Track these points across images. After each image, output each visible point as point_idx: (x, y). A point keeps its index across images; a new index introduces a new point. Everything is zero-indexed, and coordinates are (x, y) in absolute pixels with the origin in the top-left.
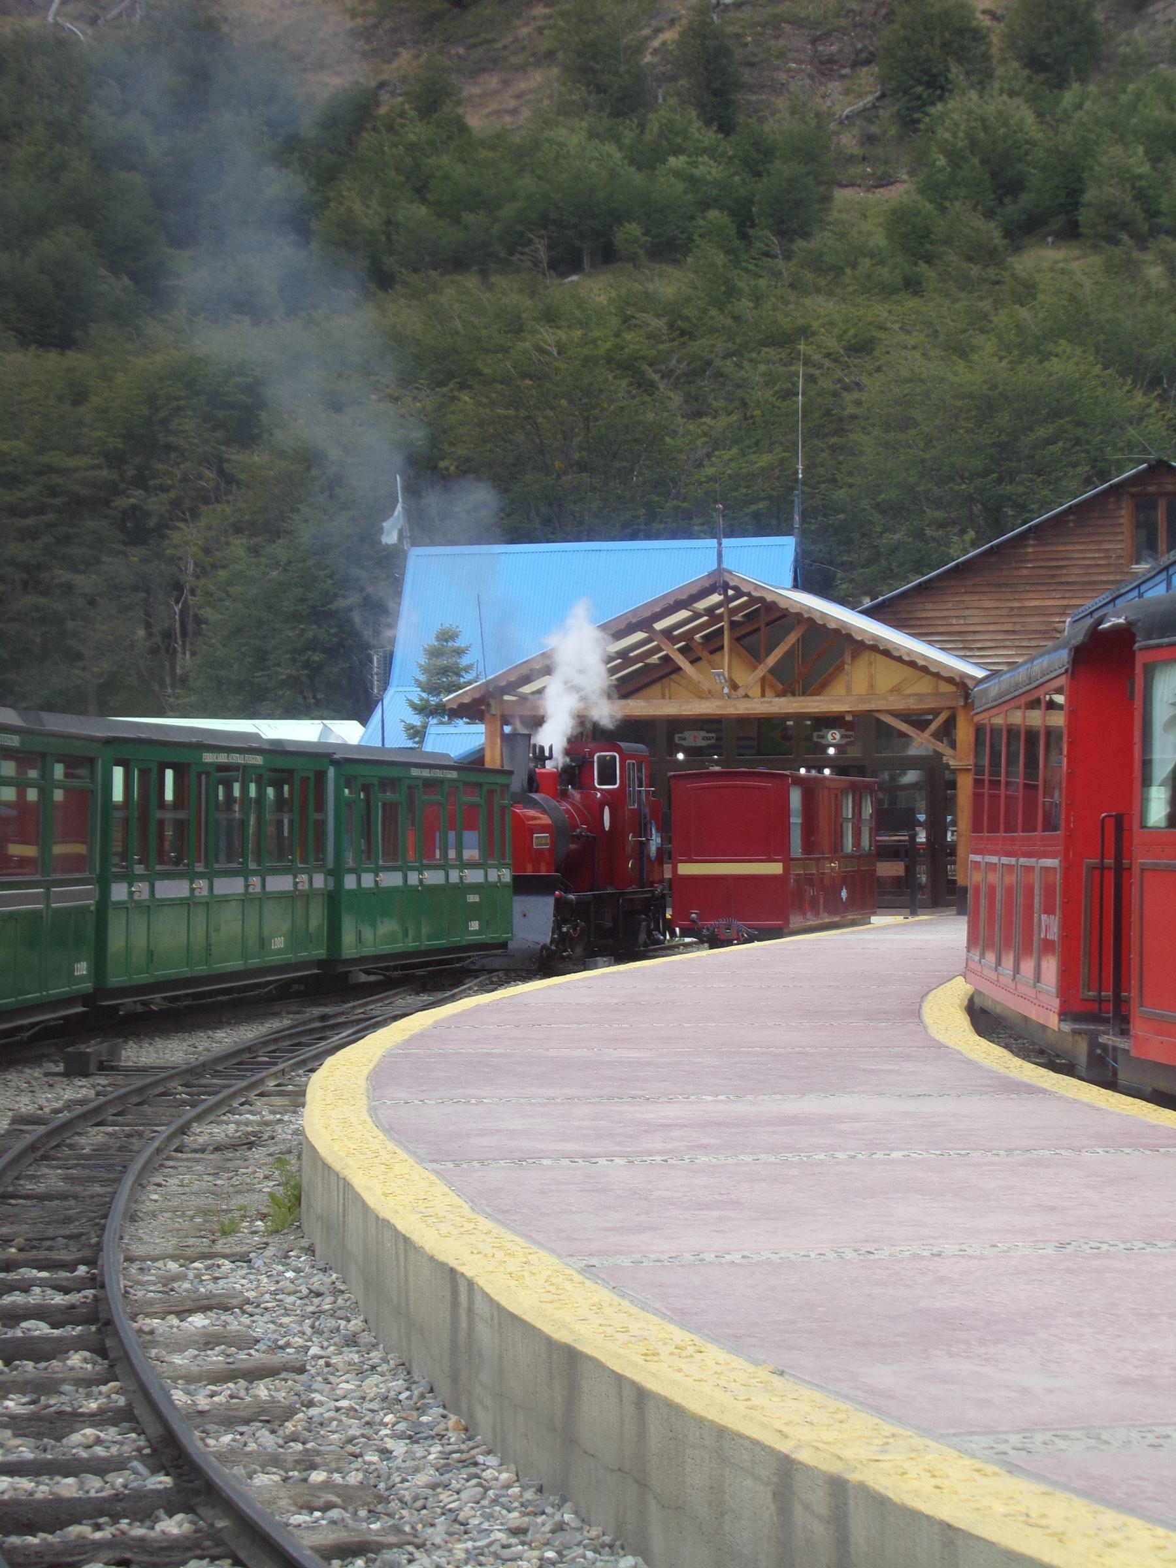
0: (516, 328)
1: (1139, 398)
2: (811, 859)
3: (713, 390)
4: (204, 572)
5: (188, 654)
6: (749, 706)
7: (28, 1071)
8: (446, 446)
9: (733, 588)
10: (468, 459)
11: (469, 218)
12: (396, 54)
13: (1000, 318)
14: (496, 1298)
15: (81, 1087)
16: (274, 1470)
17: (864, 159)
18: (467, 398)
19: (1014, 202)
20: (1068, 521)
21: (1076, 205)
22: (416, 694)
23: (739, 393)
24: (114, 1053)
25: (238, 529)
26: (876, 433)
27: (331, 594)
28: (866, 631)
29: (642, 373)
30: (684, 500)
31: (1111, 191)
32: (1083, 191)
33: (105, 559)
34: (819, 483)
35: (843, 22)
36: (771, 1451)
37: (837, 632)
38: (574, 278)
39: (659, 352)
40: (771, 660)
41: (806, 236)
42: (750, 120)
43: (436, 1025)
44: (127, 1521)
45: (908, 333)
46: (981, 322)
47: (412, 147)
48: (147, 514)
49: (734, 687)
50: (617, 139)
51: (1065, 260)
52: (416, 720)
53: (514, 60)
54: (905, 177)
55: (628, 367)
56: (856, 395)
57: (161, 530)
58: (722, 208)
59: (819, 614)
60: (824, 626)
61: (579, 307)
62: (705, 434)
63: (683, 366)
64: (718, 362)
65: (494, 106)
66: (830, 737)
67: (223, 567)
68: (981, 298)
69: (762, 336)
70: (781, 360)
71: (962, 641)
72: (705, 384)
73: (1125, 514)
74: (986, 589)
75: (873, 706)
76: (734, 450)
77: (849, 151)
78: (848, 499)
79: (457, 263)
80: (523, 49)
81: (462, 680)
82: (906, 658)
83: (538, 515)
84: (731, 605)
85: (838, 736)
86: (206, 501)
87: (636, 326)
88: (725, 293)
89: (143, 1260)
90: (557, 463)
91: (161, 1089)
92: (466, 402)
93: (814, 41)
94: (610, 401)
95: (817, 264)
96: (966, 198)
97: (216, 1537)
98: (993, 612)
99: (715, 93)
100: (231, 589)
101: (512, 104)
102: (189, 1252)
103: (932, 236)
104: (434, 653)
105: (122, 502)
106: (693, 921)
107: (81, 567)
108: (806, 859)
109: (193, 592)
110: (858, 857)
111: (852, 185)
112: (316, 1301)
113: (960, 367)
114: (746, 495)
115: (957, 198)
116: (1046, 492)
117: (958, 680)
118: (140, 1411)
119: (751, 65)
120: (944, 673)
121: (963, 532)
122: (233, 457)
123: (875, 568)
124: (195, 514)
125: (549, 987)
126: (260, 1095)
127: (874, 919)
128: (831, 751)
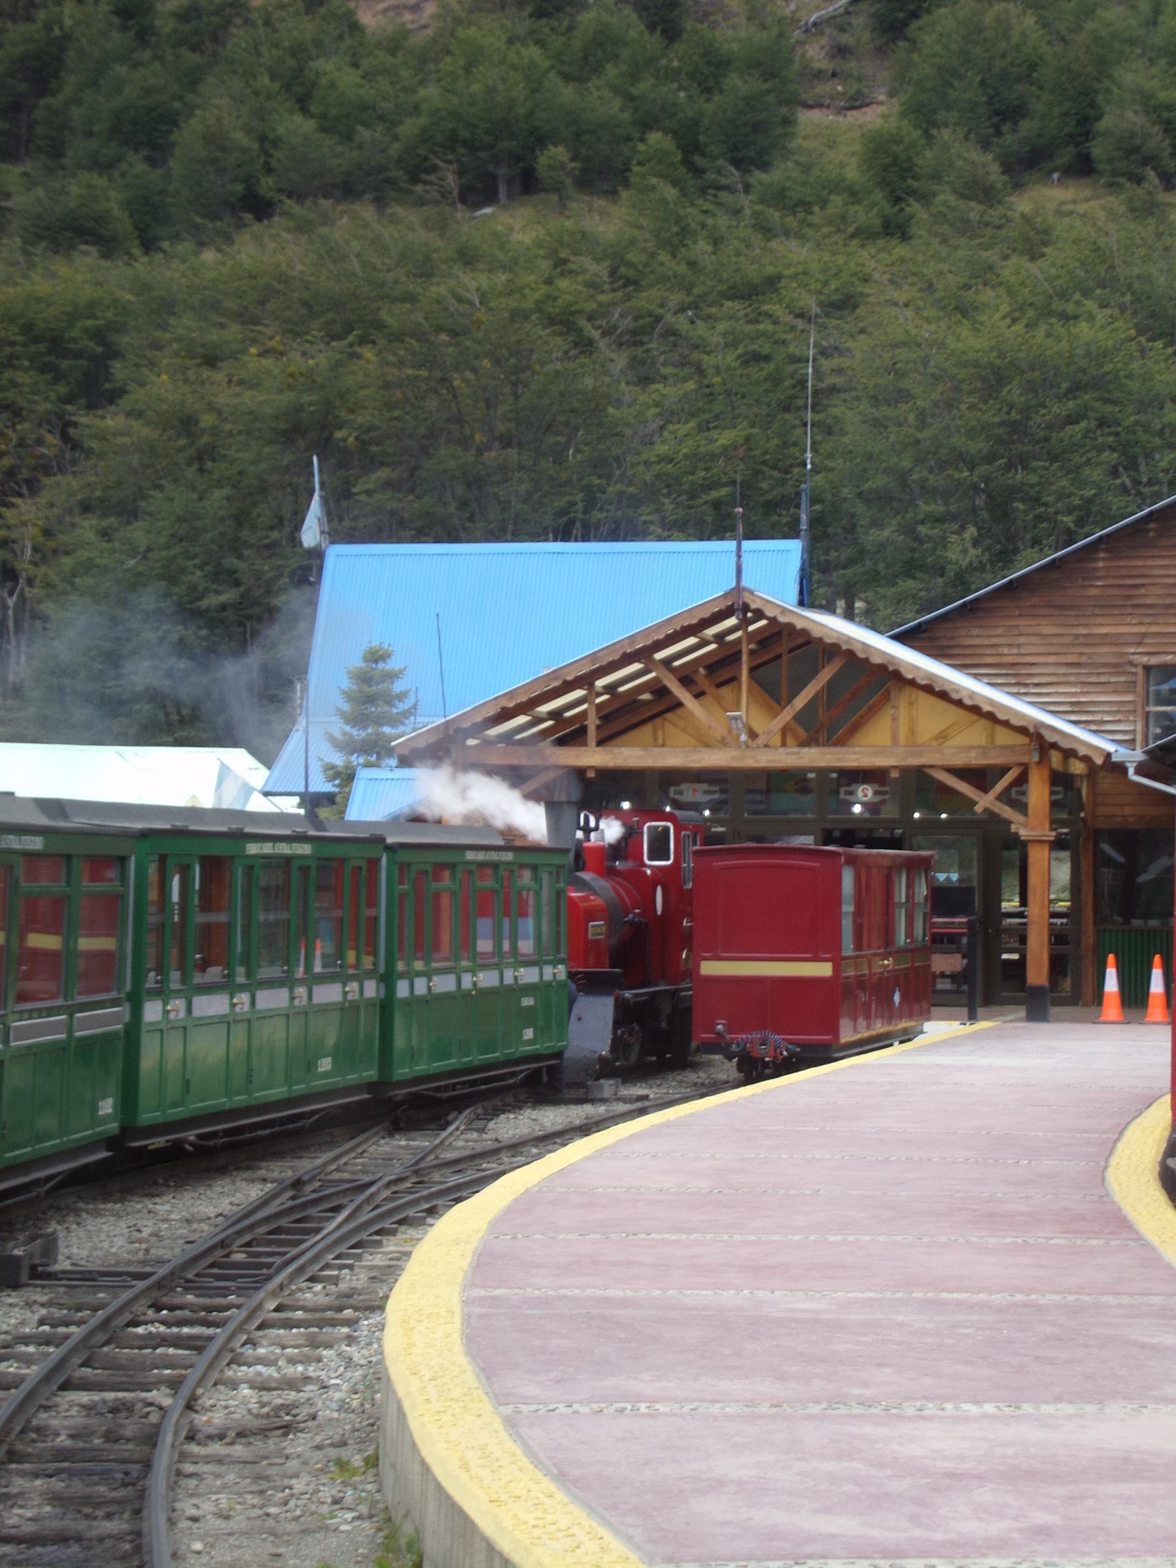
0: (425, 271)
2: (862, 956)
3: (663, 353)
4: (44, 560)
5: (23, 657)
6: (770, 758)
8: (343, 414)
9: (753, 611)
10: (370, 429)
11: (364, 134)
15: (11, 1305)
17: (834, 75)
18: (369, 355)
19: (1014, 131)
20: (1148, 531)
21: (1088, 135)
22: (338, 728)
23: (695, 356)
24: (50, 1247)
25: (86, 508)
26: (862, 408)
27: (200, 588)
28: (918, 669)
29: (579, 330)
30: (630, 484)
32: (1099, 118)
34: (792, 466)
37: (882, 668)
38: (488, 210)
39: (600, 304)
40: (800, 702)
41: (764, 166)
42: (699, 26)
43: (497, 1225)
46: (984, 274)
47: (297, 50)
49: (753, 735)
50: (541, 43)
51: (1074, 202)
52: (338, 760)
54: (882, 98)
56: (836, 361)
58: (666, 131)
59: (860, 646)
60: (866, 660)
61: (501, 247)
62: (657, 405)
63: (628, 322)
64: (669, 318)
66: (860, 793)
67: (67, 553)
69: (725, 287)
70: (746, 315)
71: (1016, 675)
74: (1043, 611)
76: (692, 424)
77: (816, 65)
78: (827, 487)
79: (347, 190)
81: (395, 711)
82: (968, 702)
83: (454, 498)
84: (751, 628)
85: (870, 793)
86: (47, 471)
87: (570, 271)
88: (677, 234)
90: (477, 436)
91: (127, 1317)
92: (368, 361)
94: (543, 363)
95: (778, 197)
96: (956, 124)
98: (1054, 640)
100: (78, 580)
103: (917, 169)
106: (719, 1034)
108: (857, 957)
110: (912, 951)
111: (820, 106)
114: (705, 479)
115: (946, 125)
116: (1064, 482)
117: (1032, 730)
120: (1015, 722)
121: (963, 528)
122: (83, 420)
123: (857, 569)
124: (33, 487)
125: (599, 1154)
126: (260, 1328)
127: (928, 1026)
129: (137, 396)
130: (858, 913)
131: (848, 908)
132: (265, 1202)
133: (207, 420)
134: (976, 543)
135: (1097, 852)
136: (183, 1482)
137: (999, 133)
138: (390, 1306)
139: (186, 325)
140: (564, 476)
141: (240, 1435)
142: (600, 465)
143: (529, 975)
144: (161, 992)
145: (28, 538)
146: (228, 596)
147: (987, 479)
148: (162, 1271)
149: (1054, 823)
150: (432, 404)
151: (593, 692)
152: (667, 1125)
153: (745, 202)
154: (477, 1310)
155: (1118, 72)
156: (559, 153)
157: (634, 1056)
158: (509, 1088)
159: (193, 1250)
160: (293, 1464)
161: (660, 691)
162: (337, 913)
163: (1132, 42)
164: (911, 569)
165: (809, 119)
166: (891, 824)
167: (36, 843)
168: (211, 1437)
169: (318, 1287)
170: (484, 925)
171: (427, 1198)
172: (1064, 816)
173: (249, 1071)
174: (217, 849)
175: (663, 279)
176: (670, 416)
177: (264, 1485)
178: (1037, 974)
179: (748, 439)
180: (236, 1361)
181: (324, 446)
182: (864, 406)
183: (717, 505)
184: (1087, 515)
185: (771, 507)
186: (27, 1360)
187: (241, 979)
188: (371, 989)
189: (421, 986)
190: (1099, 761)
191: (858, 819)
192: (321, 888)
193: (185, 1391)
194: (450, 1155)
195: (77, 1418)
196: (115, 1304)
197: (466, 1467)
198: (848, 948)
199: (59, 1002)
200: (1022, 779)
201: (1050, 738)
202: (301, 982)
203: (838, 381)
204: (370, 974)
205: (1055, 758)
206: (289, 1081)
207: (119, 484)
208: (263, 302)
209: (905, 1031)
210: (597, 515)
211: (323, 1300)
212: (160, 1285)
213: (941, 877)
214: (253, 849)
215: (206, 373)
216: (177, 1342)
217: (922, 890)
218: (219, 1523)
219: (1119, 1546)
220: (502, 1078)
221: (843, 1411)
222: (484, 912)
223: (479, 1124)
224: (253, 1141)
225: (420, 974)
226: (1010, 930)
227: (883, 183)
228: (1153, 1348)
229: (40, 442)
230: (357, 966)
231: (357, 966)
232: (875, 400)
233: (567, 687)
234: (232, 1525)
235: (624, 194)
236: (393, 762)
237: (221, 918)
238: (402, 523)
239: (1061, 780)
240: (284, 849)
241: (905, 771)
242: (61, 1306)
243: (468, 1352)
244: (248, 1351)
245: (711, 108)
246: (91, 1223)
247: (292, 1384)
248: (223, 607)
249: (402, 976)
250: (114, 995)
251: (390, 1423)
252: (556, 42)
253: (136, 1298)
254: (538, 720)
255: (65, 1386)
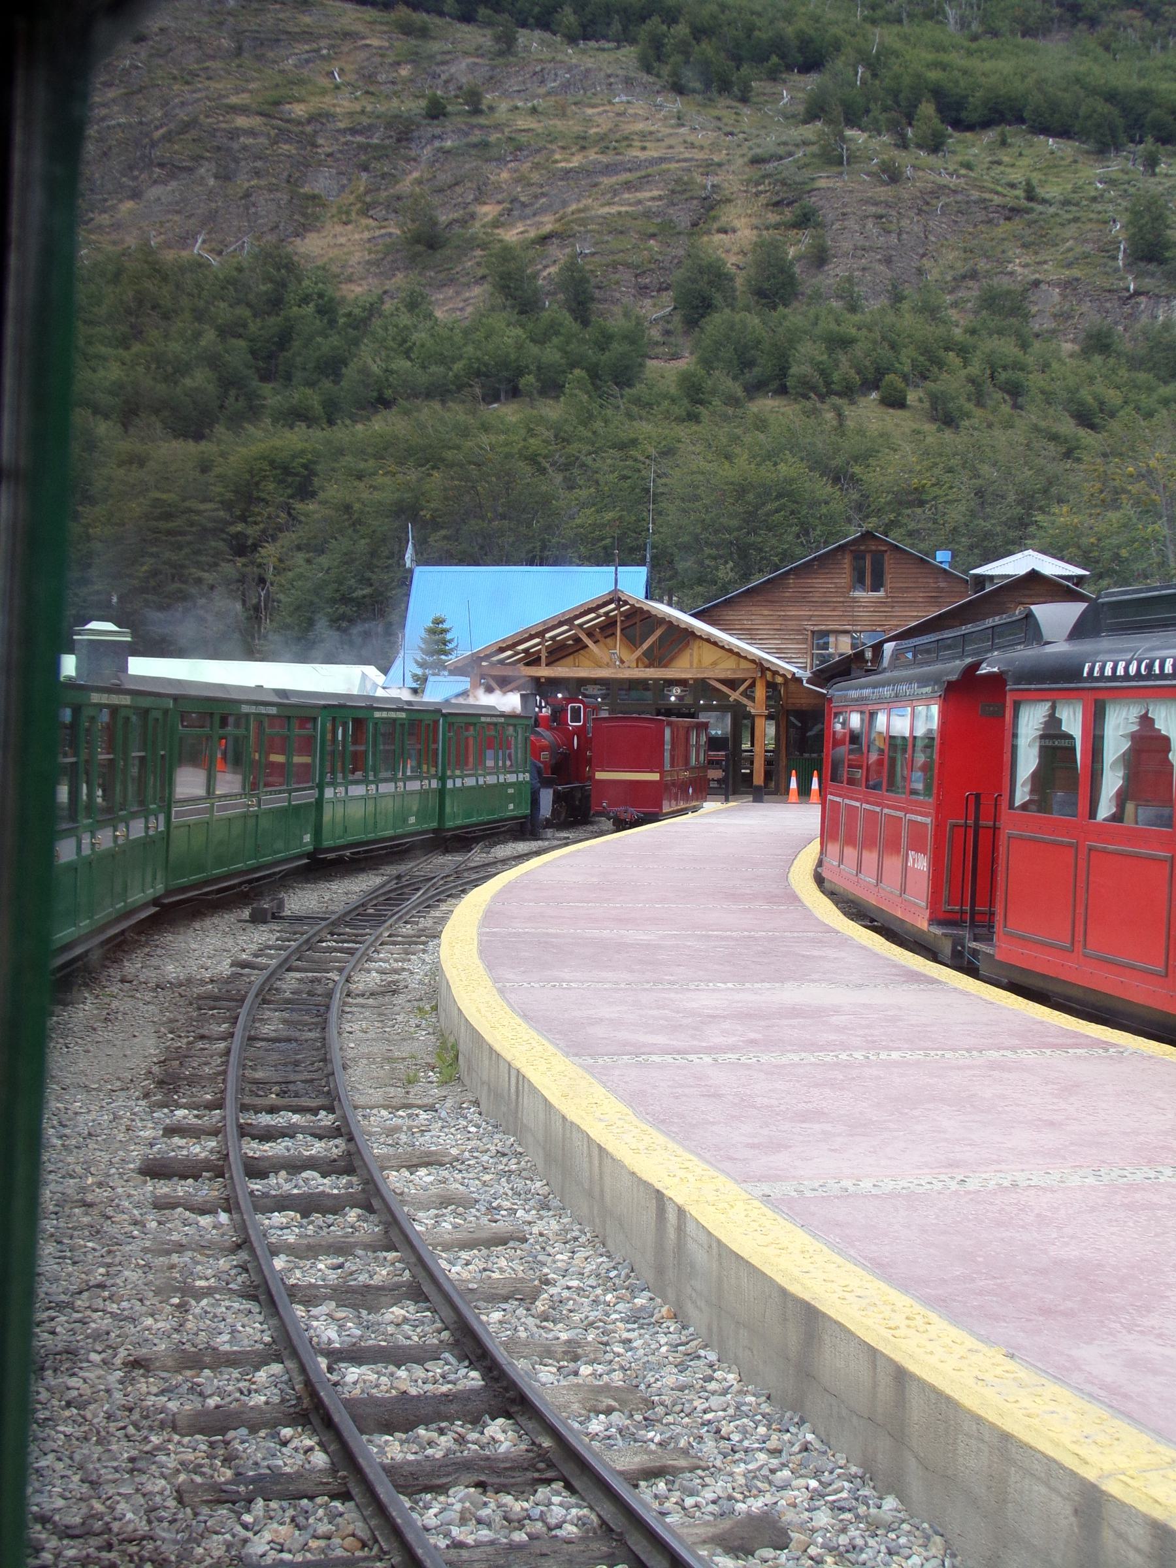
0: (465, 433)
1: (829, 489)
4: (279, 573)
7: (226, 916)
10: (437, 510)
12: (394, 275)
13: (747, 439)
14: (715, 1233)
16: (550, 1361)
21: (785, 375)
22: (420, 656)
25: (299, 548)
29: (539, 463)
31: (806, 369)
33: (223, 564)
35: (653, 266)
36: (1073, 1474)
37: (686, 630)
38: (495, 405)
40: (645, 646)
41: (630, 386)
43: (496, 898)
44: (460, 1423)
45: (694, 445)
46: (736, 439)
48: (246, 537)
49: (622, 662)
50: (522, 326)
53: (463, 280)
55: (532, 459)
56: (664, 480)
57: (255, 547)
63: (563, 460)
65: (451, 306)
68: (735, 427)
72: (576, 471)
73: (847, 562)
75: (705, 675)
79: (428, 395)
80: (468, 274)
86: (281, 531)
89: (364, 1108)
91: (318, 938)
93: (636, 276)
95: (637, 401)
97: (542, 1455)
99: (580, 303)
101: (461, 305)
102: (395, 1102)
104: (432, 632)
105: (233, 529)
107: (206, 568)
109: (272, 584)
112: (504, 1160)
113: (727, 465)
118: (427, 1288)
119: (599, 288)
121: (726, 562)
124: (274, 539)
125: (545, 864)
127: (705, 804)
128: (673, 699)
129: (322, 495)
130: (673, 749)
131: (667, 747)
132: (383, 886)
133: (357, 506)
134: (732, 570)
135: (788, 720)
136: (345, 1016)
137: (743, 373)
138: (443, 936)
139: (348, 460)
140: (531, 534)
141: (372, 994)
142: (548, 528)
143: (512, 778)
144: (333, 784)
145: (271, 563)
146: (367, 591)
147: (737, 539)
148: (334, 917)
149: (768, 707)
150: (467, 498)
151: (544, 640)
152: (578, 851)
153: (621, 402)
154: (485, 938)
155: (799, 347)
156: (531, 378)
157: (562, 818)
158: (504, 832)
159: (349, 908)
160: (397, 1009)
161: (577, 640)
162: (419, 746)
163: (805, 332)
164: (700, 581)
165: (651, 364)
166: (689, 707)
167: (273, 711)
168: (358, 995)
169: (409, 926)
170: (490, 753)
171: (461, 885)
172: (772, 703)
173: (376, 822)
174: (361, 715)
175: (580, 439)
176: (583, 505)
177: (383, 1018)
178: (758, 780)
179: (620, 517)
180: (369, 960)
181: (415, 518)
182: (678, 502)
183: (605, 548)
184: (785, 556)
185: (632, 550)
186: (271, 957)
187: (371, 778)
188: (434, 784)
189: (458, 783)
190: (789, 677)
191: (673, 704)
192: (410, 734)
193: (345, 974)
194: (473, 865)
195: (295, 985)
196: (311, 932)
197: (479, 1011)
198: (667, 767)
199: (285, 787)
200: (753, 685)
201: (766, 665)
202: (400, 780)
203: (665, 490)
204: (434, 776)
205: (769, 674)
206: (394, 828)
207: (315, 537)
208: (385, 449)
209: (694, 807)
210: (547, 553)
211: (411, 932)
212: (333, 923)
213: (713, 732)
214: (377, 714)
215: (356, 483)
216: (341, 950)
217: (704, 739)
218: (364, 1035)
219: (789, 1048)
220: (498, 827)
221: (661, 987)
222: (490, 747)
223: (486, 850)
224: (376, 856)
225: (458, 777)
226: (746, 759)
227: (688, 396)
228: (807, 957)
229: (278, 517)
230: (428, 772)
231: (428, 772)
232: (683, 500)
233: (531, 637)
234: (369, 1036)
235: (562, 399)
236: (446, 673)
237: (363, 748)
238: (452, 556)
239: (771, 685)
240: (393, 715)
241: (696, 680)
242: (286, 932)
243: (481, 958)
244: (375, 955)
245: (605, 357)
246: (300, 893)
247: (396, 971)
248: (364, 597)
249: (450, 777)
250: (310, 784)
251: (443, 990)
252: (530, 326)
253: (321, 929)
254: (517, 653)
255: (289, 970)
